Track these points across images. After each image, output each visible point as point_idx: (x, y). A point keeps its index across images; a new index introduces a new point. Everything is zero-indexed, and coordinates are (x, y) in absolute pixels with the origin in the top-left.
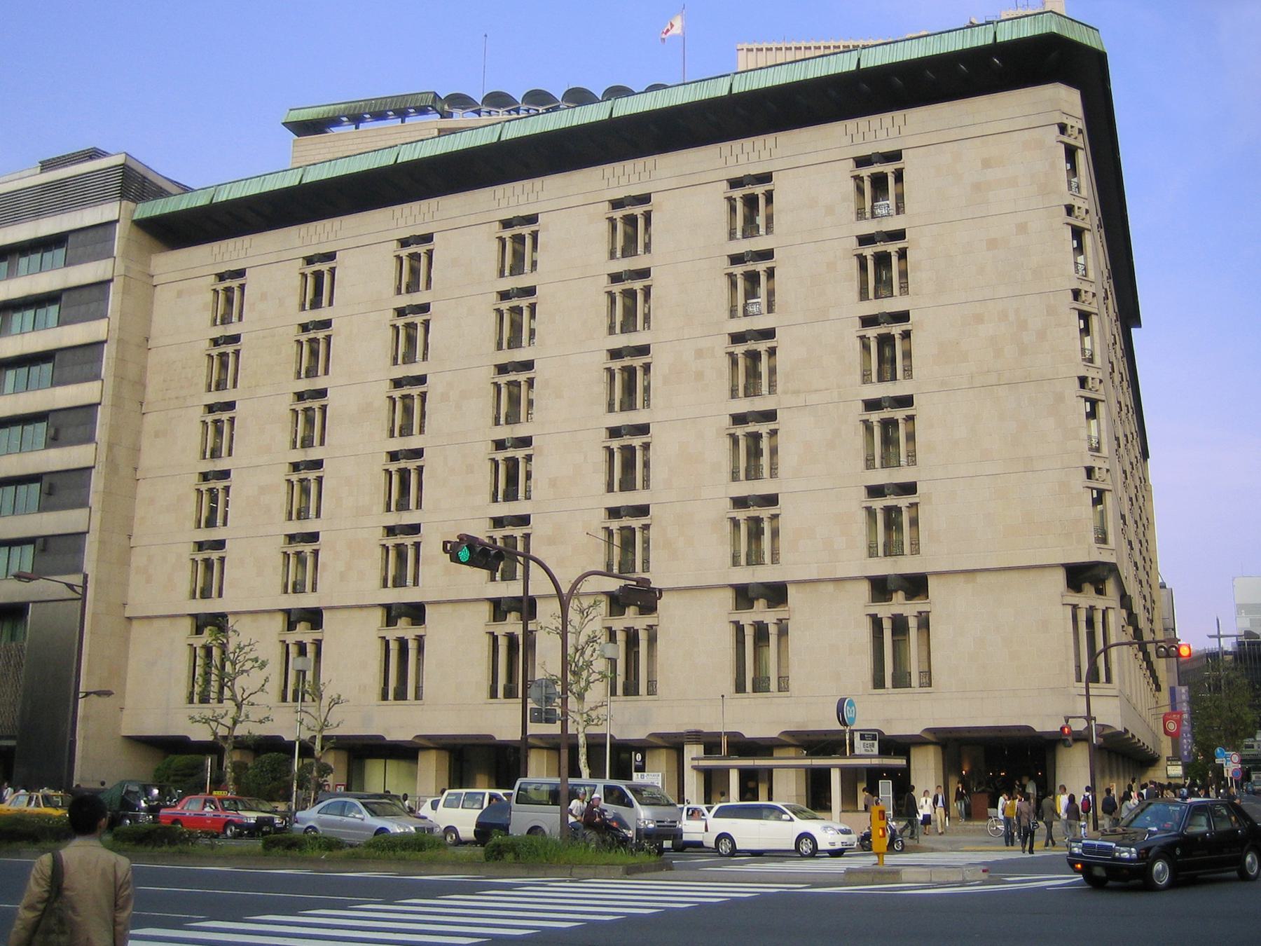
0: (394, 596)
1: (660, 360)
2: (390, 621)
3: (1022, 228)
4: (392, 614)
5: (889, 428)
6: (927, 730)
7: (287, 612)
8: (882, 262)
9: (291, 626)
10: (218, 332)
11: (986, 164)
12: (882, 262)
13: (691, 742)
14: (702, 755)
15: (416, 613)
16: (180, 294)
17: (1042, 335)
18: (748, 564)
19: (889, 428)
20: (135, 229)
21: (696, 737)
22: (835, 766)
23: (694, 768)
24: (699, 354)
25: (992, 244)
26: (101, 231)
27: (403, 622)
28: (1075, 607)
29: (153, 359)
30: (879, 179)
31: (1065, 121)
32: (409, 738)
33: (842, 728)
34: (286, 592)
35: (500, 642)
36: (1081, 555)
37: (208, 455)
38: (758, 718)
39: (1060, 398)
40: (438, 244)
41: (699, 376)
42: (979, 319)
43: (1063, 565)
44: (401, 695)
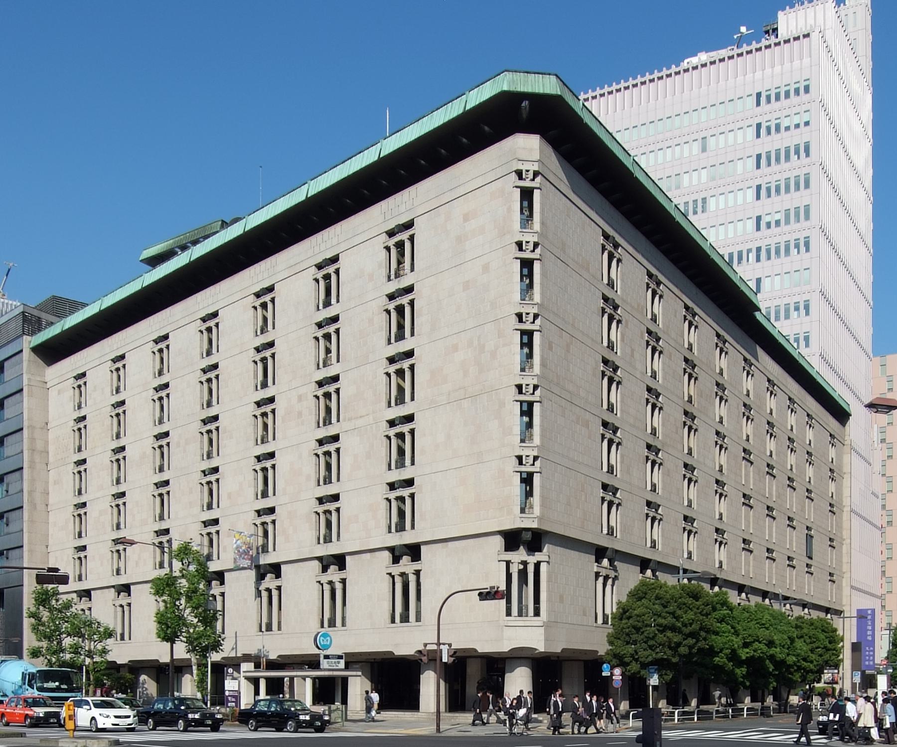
0: (396, 540)
1: (280, 405)
2: (396, 560)
3: (486, 268)
4: (396, 554)
5: (402, 436)
6: (279, 656)
7: (392, 549)
8: (401, 311)
9: (396, 560)
10: (393, 287)
11: (466, 218)
12: (401, 311)
13: (244, 661)
14: (253, 669)
15: (414, 552)
16: (59, 393)
17: (493, 354)
18: (325, 542)
19: (402, 436)
20: (32, 353)
21: (247, 658)
22: (262, 677)
23: (247, 678)
24: (300, 398)
25: (466, 286)
26: (17, 357)
27: (405, 559)
28: (508, 563)
29: (51, 436)
30: (401, 242)
31: (520, 168)
32: (412, 653)
33: (317, 651)
34: (390, 532)
35: (396, 580)
36: (515, 521)
37: (259, 442)
38: (405, 642)
39: (502, 404)
40: (342, 264)
41: (300, 414)
42: (455, 348)
43: (500, 533)
44: (405, 618)
